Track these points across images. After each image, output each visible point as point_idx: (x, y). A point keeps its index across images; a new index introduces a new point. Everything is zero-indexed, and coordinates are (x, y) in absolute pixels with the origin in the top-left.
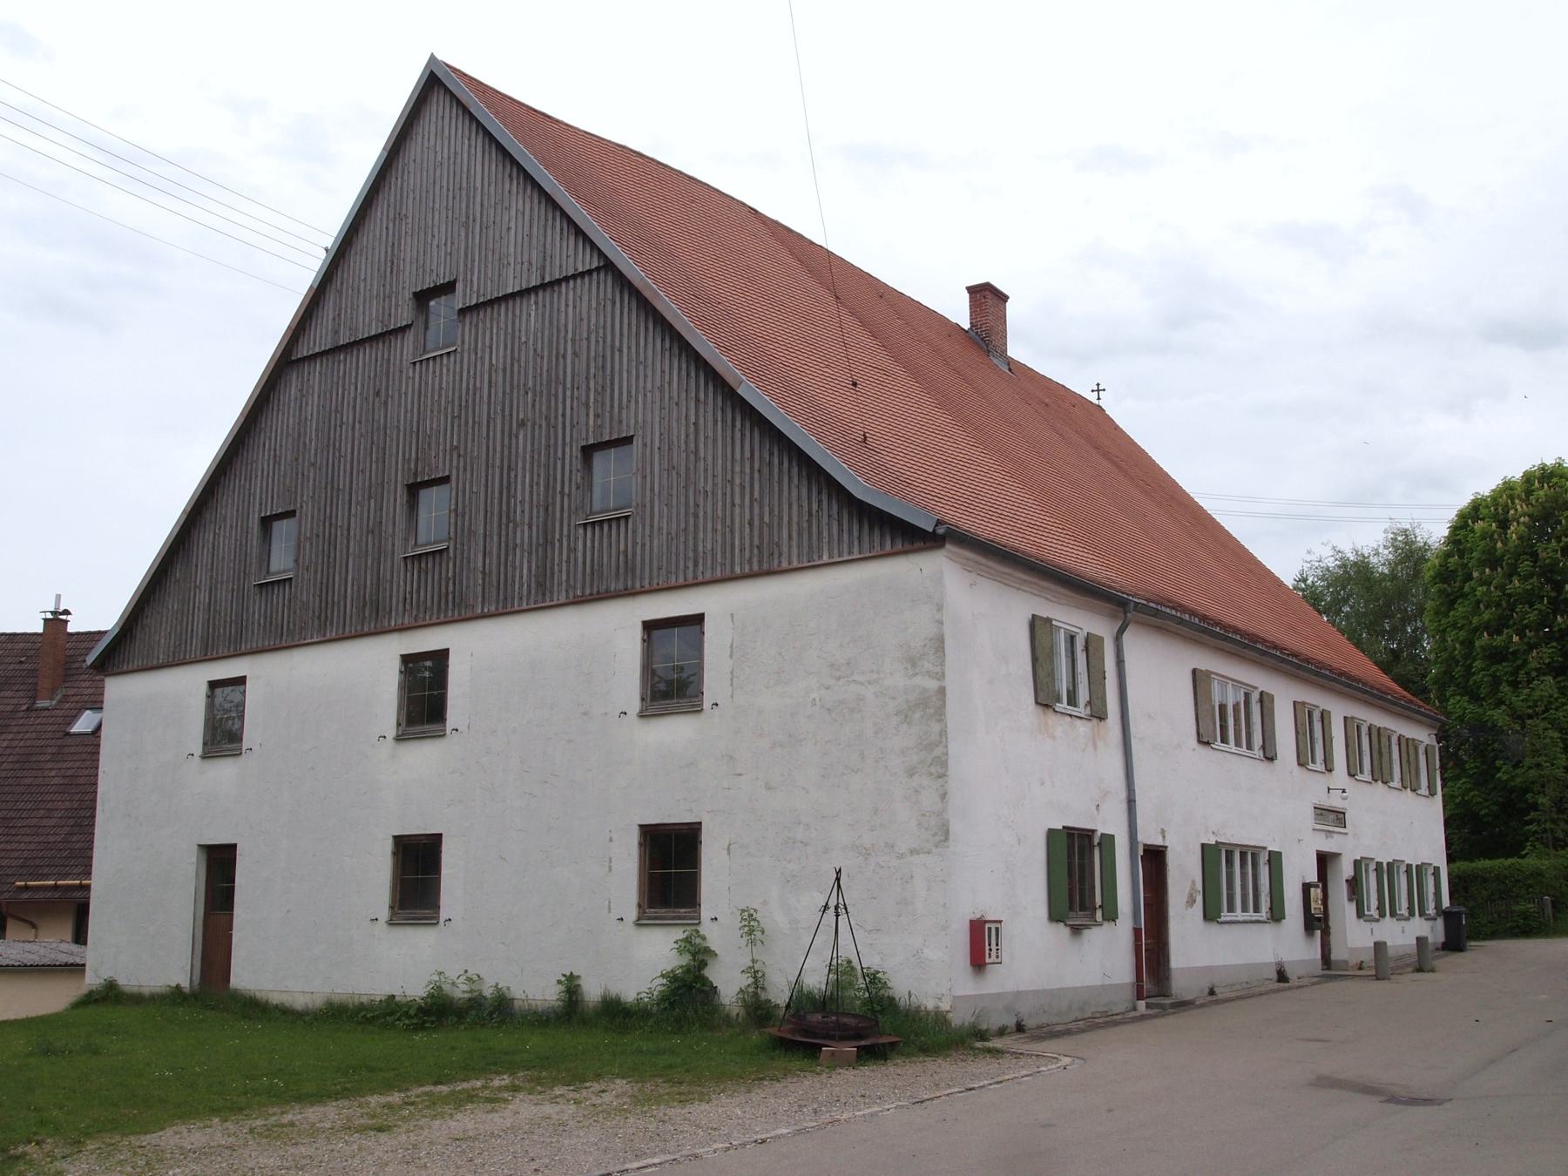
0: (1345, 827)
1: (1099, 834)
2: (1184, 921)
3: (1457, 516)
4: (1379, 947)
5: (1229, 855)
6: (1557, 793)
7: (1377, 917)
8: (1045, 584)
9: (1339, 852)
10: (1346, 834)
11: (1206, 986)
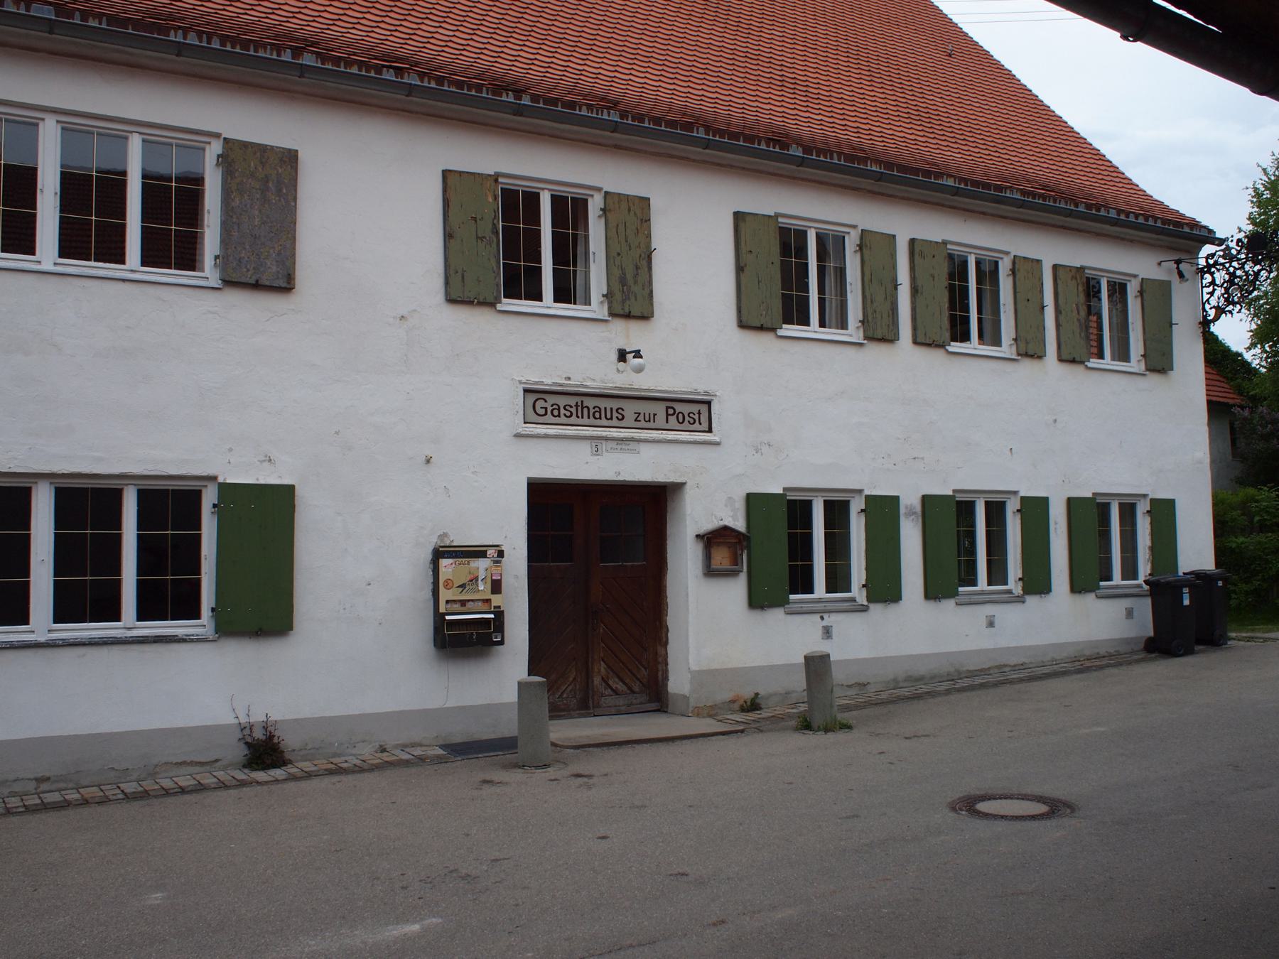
0: (710, 431)
4: (817, 666)
5: (1128, 511)
7: (865, 603)
8: (215, 82)
9: (679, 480)
10: (718, 444)
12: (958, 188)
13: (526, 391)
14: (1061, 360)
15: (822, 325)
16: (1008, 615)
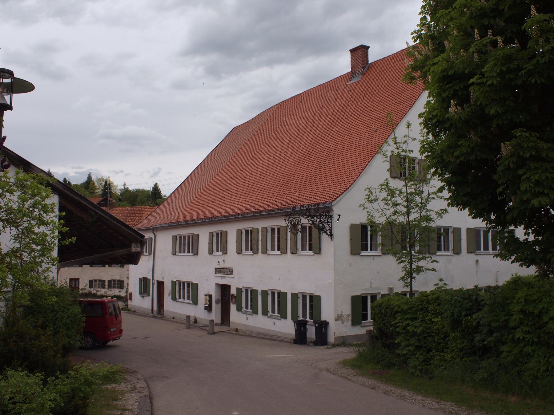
1: (260, 291)
2: (168, 299)
3: (418, 36)
6: (8, 197)
10: (234, 277)
11: (173, 316)
12: (315, 208)
13: (215, 268)
14: (262, 253)
15: (371, 250)
16: (278, 322)
